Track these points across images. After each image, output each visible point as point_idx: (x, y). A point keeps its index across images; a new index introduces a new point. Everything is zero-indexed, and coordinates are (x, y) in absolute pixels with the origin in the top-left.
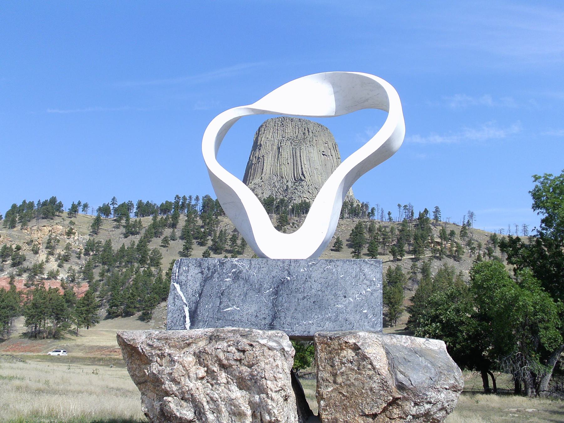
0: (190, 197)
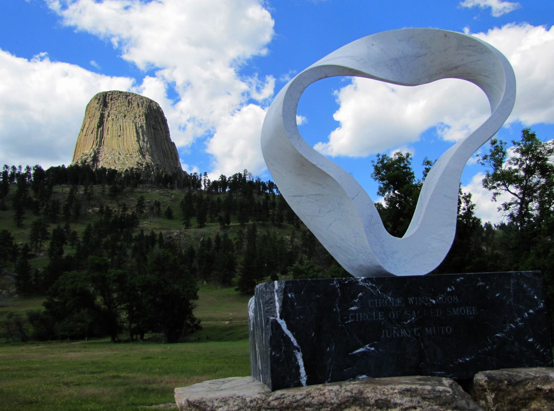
0: (20, 167)
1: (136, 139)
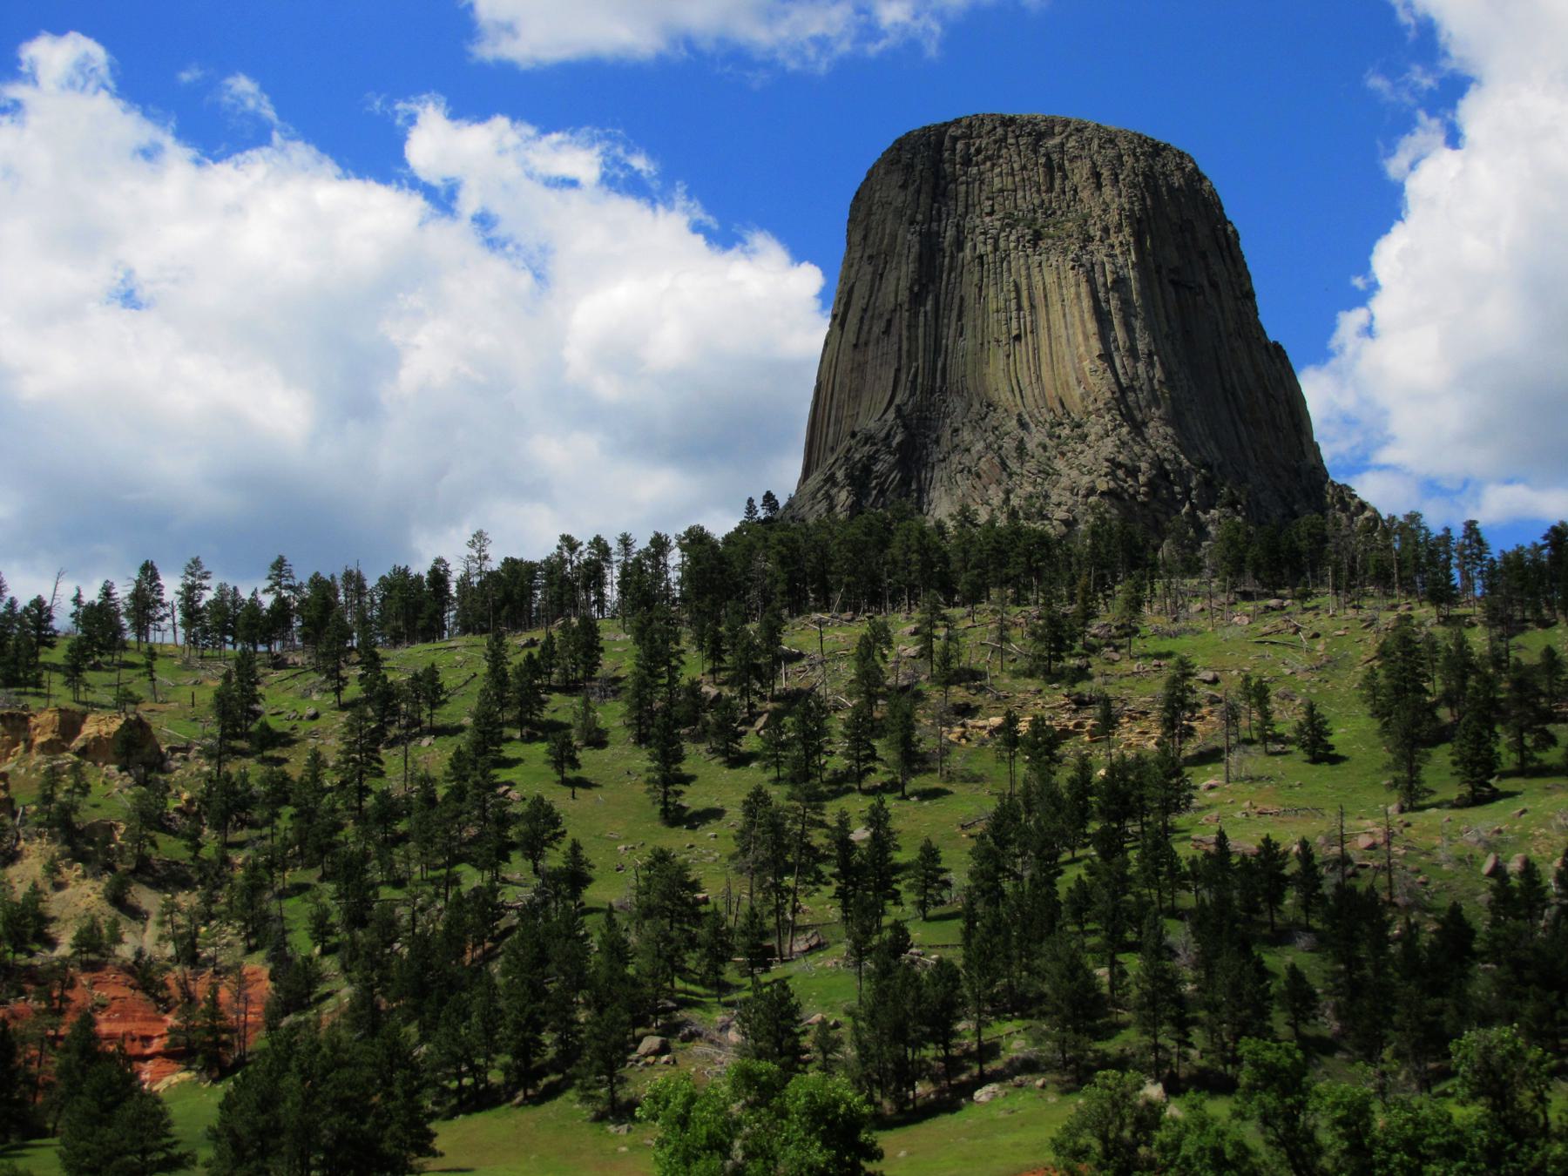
1: (1096, 346)
